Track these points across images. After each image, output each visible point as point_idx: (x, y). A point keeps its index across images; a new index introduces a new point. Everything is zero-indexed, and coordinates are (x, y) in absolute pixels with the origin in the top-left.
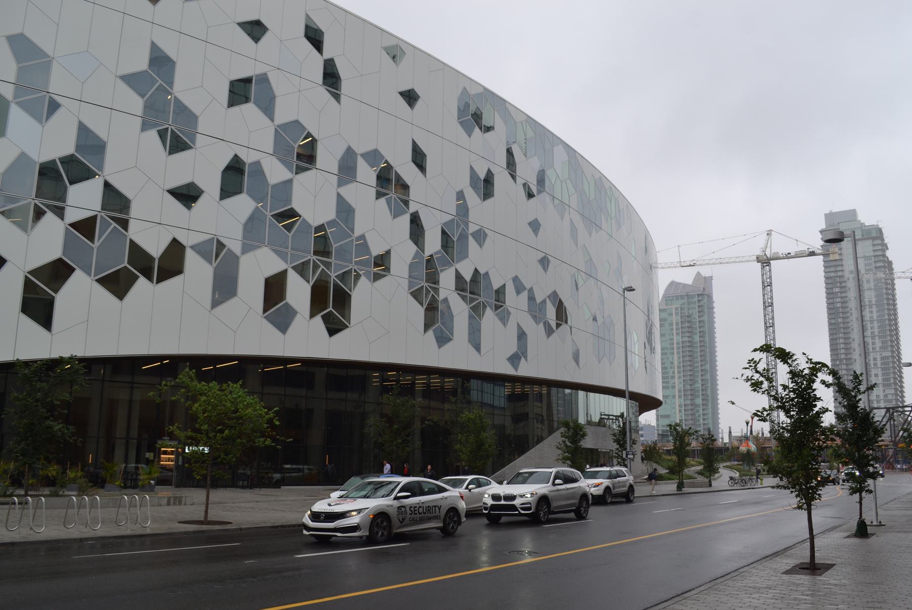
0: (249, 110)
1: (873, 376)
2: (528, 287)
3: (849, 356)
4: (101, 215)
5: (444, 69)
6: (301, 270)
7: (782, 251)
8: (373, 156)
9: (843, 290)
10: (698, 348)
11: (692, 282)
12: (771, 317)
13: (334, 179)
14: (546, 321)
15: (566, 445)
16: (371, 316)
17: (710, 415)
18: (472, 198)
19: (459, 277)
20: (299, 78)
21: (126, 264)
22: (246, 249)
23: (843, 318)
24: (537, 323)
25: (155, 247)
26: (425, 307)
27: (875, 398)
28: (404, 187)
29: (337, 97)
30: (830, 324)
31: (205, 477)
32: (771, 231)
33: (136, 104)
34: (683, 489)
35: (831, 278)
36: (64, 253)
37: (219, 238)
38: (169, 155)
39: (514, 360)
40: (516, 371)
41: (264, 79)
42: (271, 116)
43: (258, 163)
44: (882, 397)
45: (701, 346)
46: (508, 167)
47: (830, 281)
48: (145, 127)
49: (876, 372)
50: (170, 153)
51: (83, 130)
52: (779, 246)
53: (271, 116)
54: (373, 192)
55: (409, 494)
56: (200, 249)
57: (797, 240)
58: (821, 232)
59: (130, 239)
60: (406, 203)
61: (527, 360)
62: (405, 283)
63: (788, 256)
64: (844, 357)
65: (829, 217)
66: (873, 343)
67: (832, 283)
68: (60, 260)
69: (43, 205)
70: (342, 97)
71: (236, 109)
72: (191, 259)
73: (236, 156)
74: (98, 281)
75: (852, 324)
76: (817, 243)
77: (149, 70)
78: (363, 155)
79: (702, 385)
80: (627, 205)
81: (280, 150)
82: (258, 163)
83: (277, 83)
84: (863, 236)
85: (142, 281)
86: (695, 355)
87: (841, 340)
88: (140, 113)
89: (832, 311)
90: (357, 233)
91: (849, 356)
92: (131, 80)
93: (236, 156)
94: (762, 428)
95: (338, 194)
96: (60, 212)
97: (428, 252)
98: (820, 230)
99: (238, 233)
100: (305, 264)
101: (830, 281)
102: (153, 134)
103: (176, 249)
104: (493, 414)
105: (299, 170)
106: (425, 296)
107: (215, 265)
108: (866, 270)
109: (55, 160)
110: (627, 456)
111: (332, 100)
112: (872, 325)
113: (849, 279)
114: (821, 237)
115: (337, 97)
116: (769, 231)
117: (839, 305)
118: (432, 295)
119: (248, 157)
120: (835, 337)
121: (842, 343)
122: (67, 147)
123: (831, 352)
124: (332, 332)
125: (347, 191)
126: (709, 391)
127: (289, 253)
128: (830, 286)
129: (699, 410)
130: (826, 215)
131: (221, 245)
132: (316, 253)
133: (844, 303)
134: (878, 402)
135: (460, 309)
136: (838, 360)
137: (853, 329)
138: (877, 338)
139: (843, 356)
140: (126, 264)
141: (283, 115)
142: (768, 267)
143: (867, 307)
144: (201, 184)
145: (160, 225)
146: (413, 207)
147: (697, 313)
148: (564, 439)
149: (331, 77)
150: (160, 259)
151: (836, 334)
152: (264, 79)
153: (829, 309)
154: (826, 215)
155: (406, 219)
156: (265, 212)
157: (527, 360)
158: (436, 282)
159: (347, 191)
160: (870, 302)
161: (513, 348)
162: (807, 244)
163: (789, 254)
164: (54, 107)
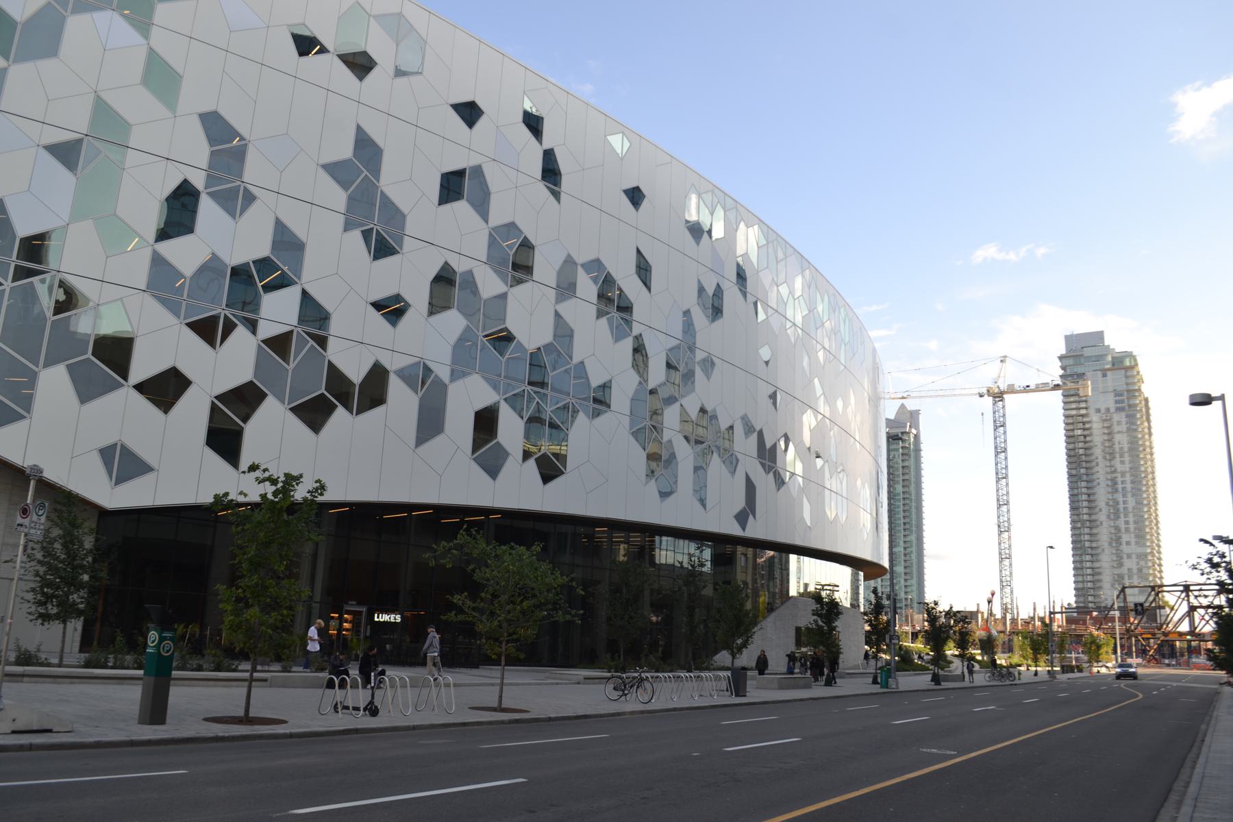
0: (461, 208)
1: (1124, 543)
2: (758, 429)
3: (1093, 517)
4: (225, 314)
5: (671, 163)
6: (514, 401)
7: (1020, 383)
8: (595, 266)
9: (1086, 433)
10: (900, 501)
12: (1004, 467)
13: (552, 294)
14: (776, 471)
15: (818, 625)
16: (588, 461)
17: (914, 588)
18: (700, 318)
20: (468, 150)
21: (323, 391)
22: (455, 376)
23: (1087, 468)
24: (767, 472)
25: (356, 372)
26: (525, 419)
27: (1126, 572)
28: (626, 308)
29: (556, 195)
30: (1070, 476)
31: (499, 656)
32: (1005, 357)
33: (338, 197)
34: (942, 683)
35: (1072, 416)
36: (256, 375)
37: (427, 362)
38: (374, 260)
39: (742, 518)
40: (744, 529)
41: (478, 171)
42: (485, 216)
43: (470, 273)
44: (1135, 571)
45: (904, 499)
47: (1070, 421)
48: (348, 227)
49: (1128, 540)
50: (376, 258)
51: (280, 227)
52: (1012, 376)
53: (485, 216)
56: (403, 374)
57: (1038, 370)
58: (1061, 358)
59: (329, 361)
60: (629, 323)
61: (755, 518)
62: (626, 421)
63: (1027, 389)
64: (1088, 519)
65: (1069, 339)
66: (1125, 502)
67: (1072, 424)
68: (251, 384)
69: (235, 317)
70: (563, 196)
71: (447, 207)
72: (396, 387)
73: (446, 263)
74: (292, 409)
75: (1097, 477)
76: (1054, 373)
77: (354, 159)
78: (582, 265)
79: (905, 548)
80: (861, 328)
81: (495, 260)
82: (470, 273)
83: (493, 177)
84: (1113, 365)
85: (340, 411)
86: (897, 510)
87: (1084, 496)
89: (1073, 459)
90: (576, 359)
91: (1093, 517)
92: (335, 170)
93: (446, 263)
95: (557, 314)
96: (252, 326)
98: (1059, 355)
100: (520, 395)
102: (356, 235)
103: (378, 376)
104: (659, 576)
107: (420, 394)
109: (249, 263)
110: (890, 641)
111: (552, 198)
112: (1123, 479)
114: (1060, 364)
115: (556, 195)
116: (1003, 357)
118: (538, 403)
119: (460, 265)
120: (1076, 491)
121: (1086, 501)
122: (263, 249)
123: (1070, 511)
124: (547, 478)
125: (566, 309)
126: (914, 556)
127: (185, 297)
128: (1071, 427)
129: (900, 581)
130: (1066, 337)
131: (428, 370)
132: (530, 383)
134: (1130, 577)
135: (685, 454)
136: (1079, 521)
137: (1099, 484)
138: (1129, 495)
139: (1085, 517)
140: (323, 391)
141: (499, 214)
142: (1001, 403)
145: (362, 345)
146: (636, 330)
147: (901, 456)
148: (815, 617)
149: (551, 172)
150: (362, 385)
151: (1077, 488)
152: (478, 171)
153: (1069, 456)
155: (628, 344)
156: (477, 332)
157: (755, 518)
159: (566, 309)
160: (1121, 449)
161: (740, 504)
162: (1051, 375)
163: (1028, 386)
164: (250, 198)
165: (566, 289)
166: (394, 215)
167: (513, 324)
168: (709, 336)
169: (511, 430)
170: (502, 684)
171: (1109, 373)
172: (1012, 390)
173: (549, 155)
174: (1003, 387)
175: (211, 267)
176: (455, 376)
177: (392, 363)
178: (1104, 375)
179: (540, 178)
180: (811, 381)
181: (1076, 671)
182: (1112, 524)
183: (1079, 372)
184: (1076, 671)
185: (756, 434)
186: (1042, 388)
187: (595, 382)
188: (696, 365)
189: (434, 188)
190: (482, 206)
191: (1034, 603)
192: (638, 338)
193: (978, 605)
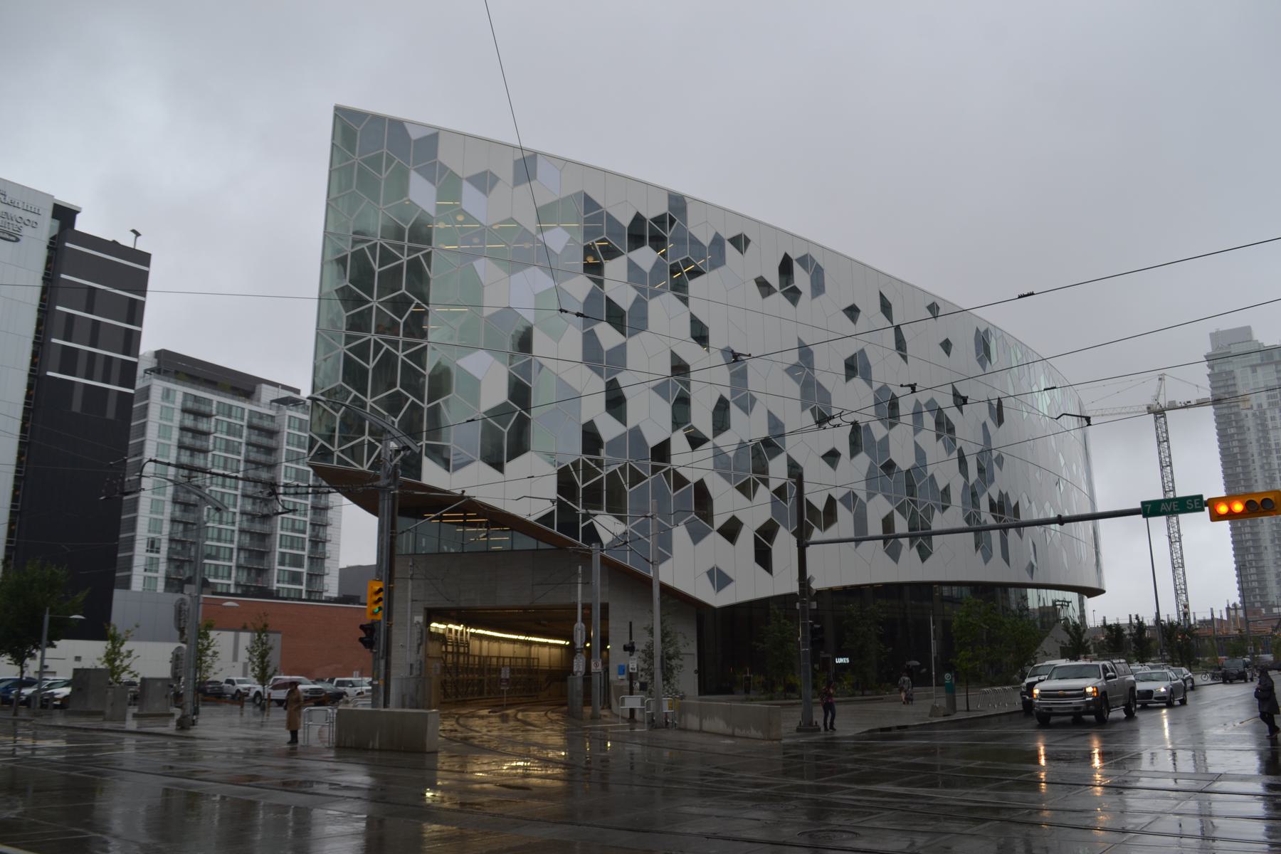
0: (858, 381)
6: (900, 509)
7: (1180, 399)
11: (1223, 488)
18: (991, 425)
19: (991, 500)
28: (951, 430)
33: (794, 389)
54: (934, 435)
57: (1197, 386)
60: (954, 440)
62: (960, 510)
67: (1224, 423)
70: (691, 300)
84: (1262, 360)
88: (728, 384)
90: (929, 474)
99: (863, 485)
101: (1222, 421)
103: (831, 502)
105: (892, 425)
106: (575, 470)
108: (1269, 404)
113: (1247, 416)
117: (1236, 450)
122: (764, 433)
131: (855, 496)
132: (754, 472)
133: (1243, 446)
142: (1163, 419)
143: (1274, 452)
144: (839, 450)
146: (959, 444)
154: (1212, 335)
155: (955, 454)
158: (766, 471)
167: (895, 456)
168: (999, 436)
169: (901, 525)
170: (967, 695)
171: (1259, 369)
172: (1173, 407)
174: (1163, 402)
175: (742, 445)
176: (869, 498)
177: (838, 494)
178: (1254, 371)
180: (1057, 456)
182: (1274, 522)
183: (1228, 369)
186: (1200, 403)
189: (842, 369)
191: (1212, 609)
192: (960, 450)
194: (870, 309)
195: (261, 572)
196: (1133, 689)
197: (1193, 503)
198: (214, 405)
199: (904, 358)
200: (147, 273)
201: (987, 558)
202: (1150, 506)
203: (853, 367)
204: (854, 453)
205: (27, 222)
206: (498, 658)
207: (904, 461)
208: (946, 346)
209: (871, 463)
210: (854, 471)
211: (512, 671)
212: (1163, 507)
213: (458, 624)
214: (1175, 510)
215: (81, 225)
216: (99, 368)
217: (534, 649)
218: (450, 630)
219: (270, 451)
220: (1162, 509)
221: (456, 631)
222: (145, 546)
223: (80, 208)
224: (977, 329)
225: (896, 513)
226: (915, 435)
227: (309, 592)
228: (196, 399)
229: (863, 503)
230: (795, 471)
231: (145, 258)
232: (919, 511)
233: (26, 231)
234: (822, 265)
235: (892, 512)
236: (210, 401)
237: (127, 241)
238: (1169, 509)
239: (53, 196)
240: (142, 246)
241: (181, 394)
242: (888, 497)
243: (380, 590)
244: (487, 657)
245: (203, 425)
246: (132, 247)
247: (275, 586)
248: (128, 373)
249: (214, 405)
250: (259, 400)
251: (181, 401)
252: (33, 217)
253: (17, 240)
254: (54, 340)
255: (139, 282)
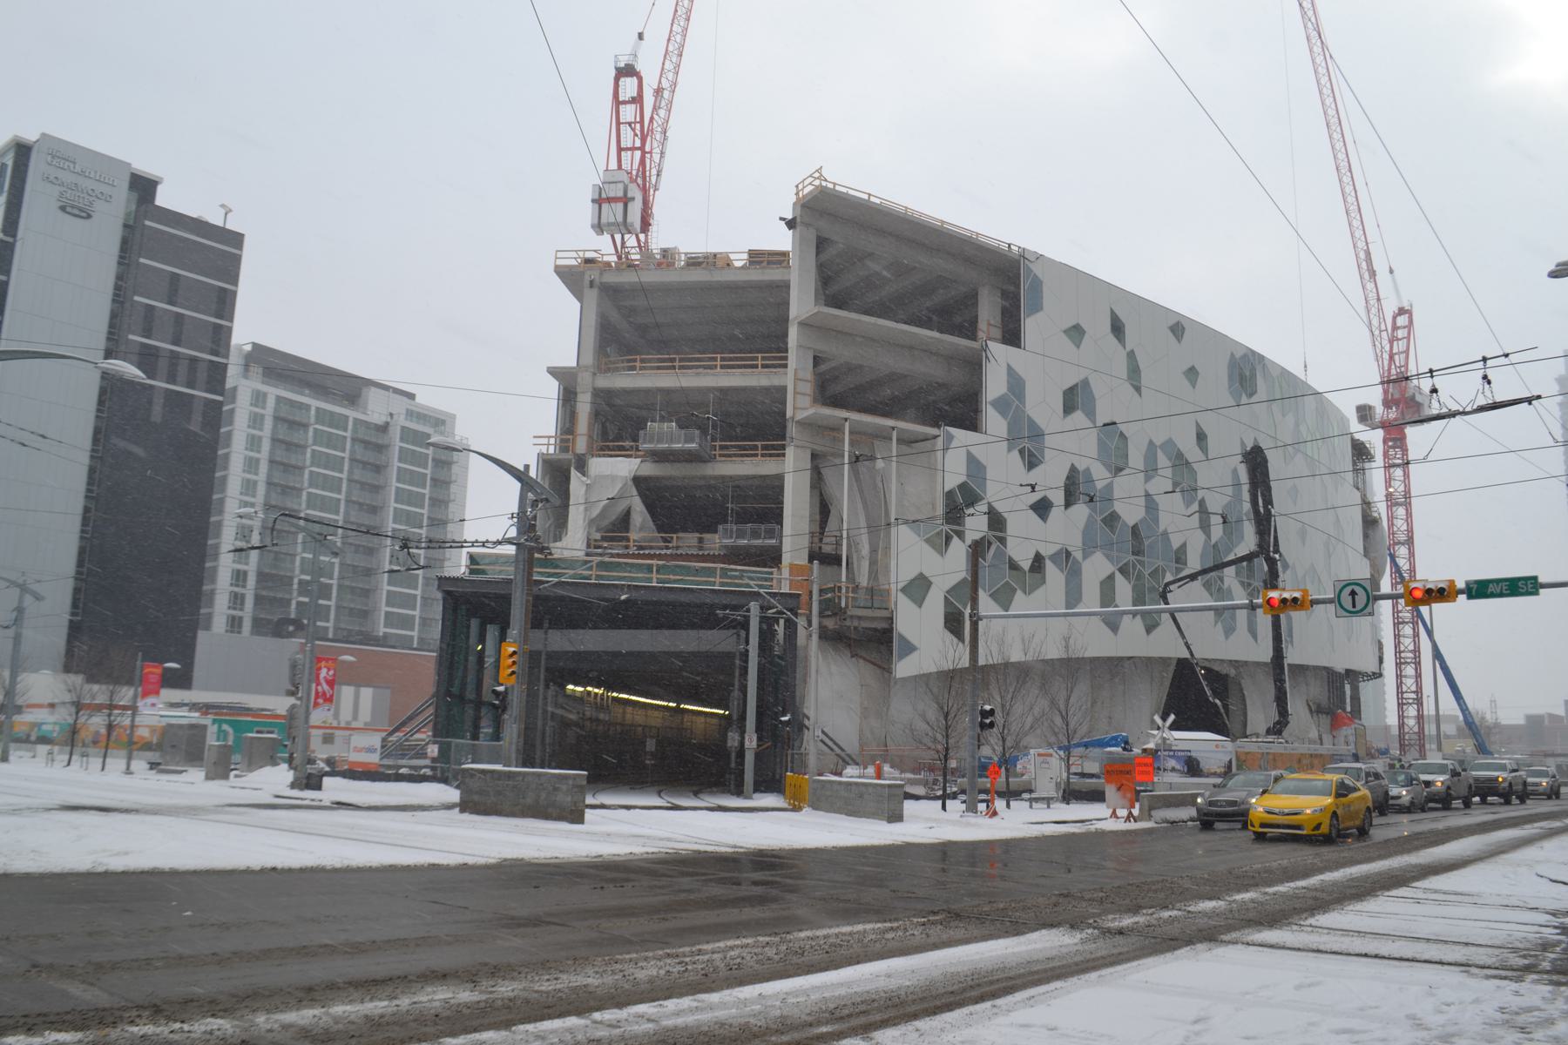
0: (1078, 417)
8: (1169, 443)
43: (1087, 470)
46: (1130, 378)
48: (1009, 450)
51: (971, 459)
55: (1440, 806)
70: (1143, 390)
82: (1087, 470)
90: (1162, 528)
94: (1493, 702)
96: (960, 535)
97: (1214, 540)
102: (1016, 453)
103: (1038, 562)
131: (1068, 554)
132: (1133, 553)
155: (1195, 507)
165: (1150, 471)
166: (1037, 434)
167: (1119, 507)
173: (1131, 355)
177: (1047, 551)
179: (1125, 377)
181: (651, 745)
184: (651, 745)
185: (1197, 503)
187: (1176, 544)
188: (1159, 450)
190: (1091, 414)
192: (1202, 503)
193: (782, 219)
194: (1099, 328)
195: (365, 614)
196: (1386, 793)
197: (1526, 585)
198: (313, 412)
199: (1138, 389)
200: (240, 256)
201: (1229, 631)
202: (1475, 586)
203: (1075, 399)
204: (1068, 504)
205: (100, 196)
206: (645, 727)
207: (1131, 513)
208: (1192, 373)
209: (1090, 516)
210: (1067, 526)
211: (659, 743)
212: (1491, 588)
213: (599, 687)
214: (1504, 592)
215: (163, 199)
216: (182, 370)
217: (686, 718)
218: (589, 693)
219: (378, 469)
220: (1490, 590)
221: (596, 694)
222: (229, 580)
223: (162, 179)
224: (1232, 354)
225: (1118, 576)
226: (1146, 482)
227: (421, 640)
228: (292, 403)
229: (1078, 562)
230: (996, 521)
231: (237, 239)
232: (1146, 574)
233: (99, 206)
234: (1040, 276)
235: (1113, 574)
236: (308, 407)
237: (216, 219)
238: (1498, 591)
239: (129, 164)
240: (232, 225)
241: (274, 397)
242: (1108, 557)
243: (514, 653)
244: (632, 725)
245: (296, 437)
246: (221, 224)
247: (382, 630)
248: (216, 376)
249: (313, 412)
250: (366, 408)
251: (273, 405)
252: (107, 190)
253: (89, 216)
254: (131, 337)
255: (229, 267)
